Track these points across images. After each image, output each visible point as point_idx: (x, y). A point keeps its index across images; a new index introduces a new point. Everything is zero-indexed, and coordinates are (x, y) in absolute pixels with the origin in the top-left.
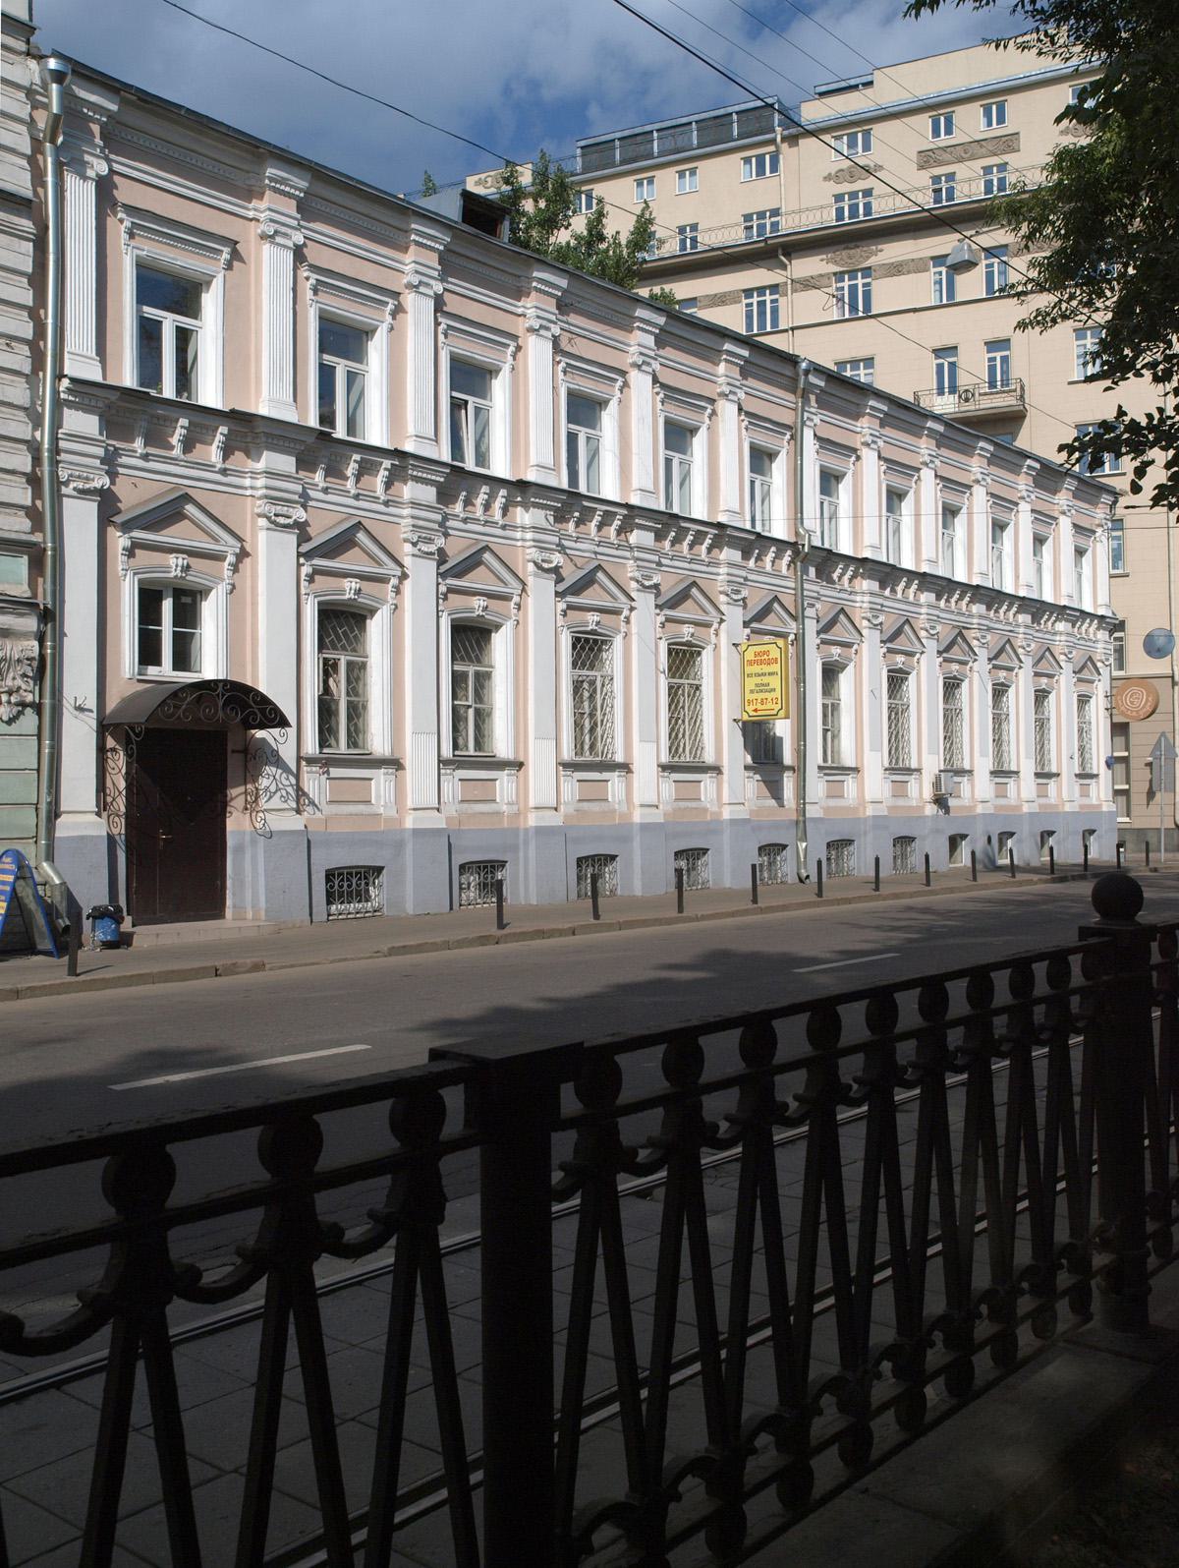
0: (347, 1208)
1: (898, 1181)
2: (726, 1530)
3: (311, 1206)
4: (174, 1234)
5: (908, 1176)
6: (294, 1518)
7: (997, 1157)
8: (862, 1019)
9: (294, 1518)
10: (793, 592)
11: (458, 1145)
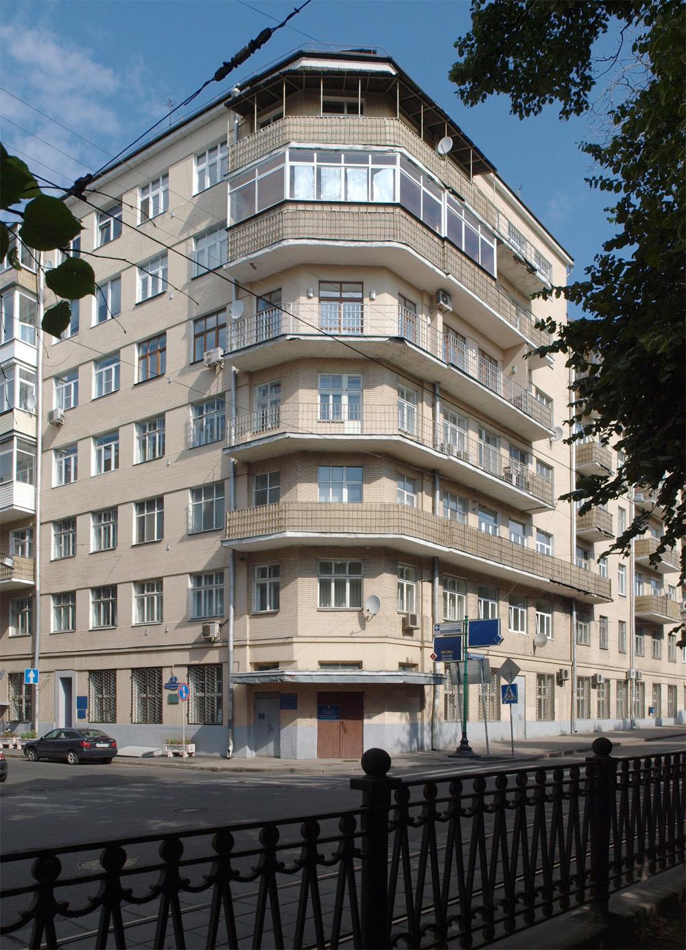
0: (193, 874)
1: (543, 852)
2: (466, 939)
3: (229, 863)
4: (278, 853)
5: (520, 861)
6: (310, 936)
7: (577, 850)
8: (337, 826)
9: (310, 936)
10: (35, 369)
11: (359, 835)
